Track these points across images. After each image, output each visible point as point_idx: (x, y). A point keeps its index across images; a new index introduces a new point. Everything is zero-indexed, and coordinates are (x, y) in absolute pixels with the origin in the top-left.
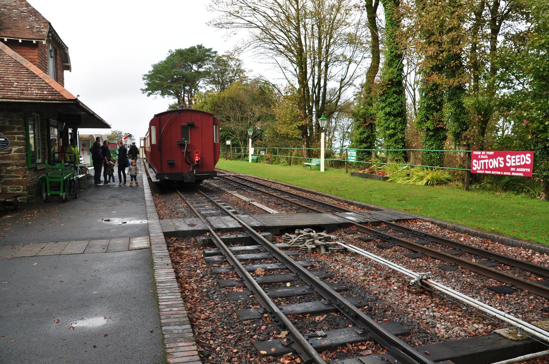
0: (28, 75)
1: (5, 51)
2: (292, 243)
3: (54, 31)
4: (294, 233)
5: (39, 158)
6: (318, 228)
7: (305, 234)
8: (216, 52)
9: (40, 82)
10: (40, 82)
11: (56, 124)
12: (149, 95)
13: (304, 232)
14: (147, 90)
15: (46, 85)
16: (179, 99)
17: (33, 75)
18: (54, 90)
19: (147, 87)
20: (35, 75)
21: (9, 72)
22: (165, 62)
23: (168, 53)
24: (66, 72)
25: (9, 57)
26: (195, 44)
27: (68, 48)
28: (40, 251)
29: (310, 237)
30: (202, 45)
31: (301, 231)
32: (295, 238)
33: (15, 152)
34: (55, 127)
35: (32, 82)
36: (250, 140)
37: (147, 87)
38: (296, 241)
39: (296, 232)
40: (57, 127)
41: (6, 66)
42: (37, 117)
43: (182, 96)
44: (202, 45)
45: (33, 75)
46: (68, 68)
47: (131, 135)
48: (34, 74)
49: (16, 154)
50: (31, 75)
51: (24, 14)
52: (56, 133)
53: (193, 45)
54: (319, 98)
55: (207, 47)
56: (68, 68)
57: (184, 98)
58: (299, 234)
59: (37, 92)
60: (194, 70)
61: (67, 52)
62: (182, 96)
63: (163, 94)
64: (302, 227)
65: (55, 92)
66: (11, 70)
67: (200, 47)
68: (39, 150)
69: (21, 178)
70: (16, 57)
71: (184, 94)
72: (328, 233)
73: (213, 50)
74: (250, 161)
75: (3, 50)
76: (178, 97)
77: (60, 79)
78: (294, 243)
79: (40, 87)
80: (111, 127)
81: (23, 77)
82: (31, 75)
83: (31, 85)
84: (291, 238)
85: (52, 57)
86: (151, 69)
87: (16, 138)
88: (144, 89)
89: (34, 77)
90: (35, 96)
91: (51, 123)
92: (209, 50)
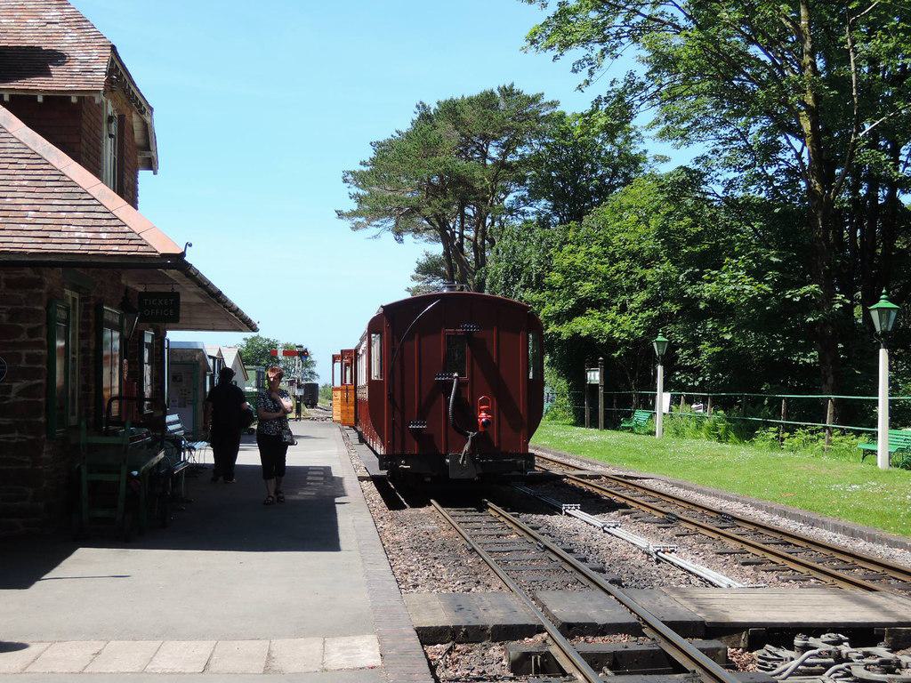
0: (63, 189)
1: (9, 130)
2: (785, 674)
3: (123, 66)
4: (791, 647)
5: (73, 414)
6: (862, 635)
7: (824, 648)
8: (554, 104)
9: (92, 208)
10: (92, 208)
11: (117, 320)
12: (356, 227)
13: (821, 643)
14: (354, 214)
15: (107, 216)
16: (447, 248)
17: (74, 190)
18: (126, 229)
19: (354, 206)
20: (80, 190)
21: (16, 183)
22: (408, 135)
23: (416, 110)
24: (144, 176)
25: (18, 145)
26: (493, 84)
27: (152, 109)
28: (92, 661)
29: (839, 658)
30: (512, 85)
31: (812, 641)
32: (792, 659)
33: (19, 394)
34: (113, 327)
35: (73, 208)
36: (660, 369)
37: (354, 206)
38: (796, 669)
39: (798, 641)
40: (119, 328)
41: (12, 166)
42: (74, 300)
43: (457, 235)
44: (512, 85)
45: (74, 190)
46: (151, 164)
47: (306, 351)
48: (78, 186)
49: (21, 399)
50: (70, 189)
51: (54, 26)
52: (117, 344)
53: (488, 88)
54: (874, 240)
55: (529, 91)
56: (151, 164)
57: (461, 245)
58: (805, 648)
59: (83, 235)
60: (492, 159)
61: (148, 120)
62: (457, 235)
63: (398, 233)
64: (815, 630)
65: (129, 236)
66: (22, 177)
67: (508, 92)
68: (73, 391)
69: (28, 467)
70: (35, 143)
71: (462, 228)
72: (894, 649)
73: (547, 99)
74: (882, 460)
75: (4, 126)
76: (447, 239)
77: (128, 191)
78: (791, 675)
79: (90, 222)
80: (258, 326)
81: (51, 196)
82: (70, 189)
83: (70, 215)
84: (781, 660)
85: (111, 136)
86: (369, 154)
87: (24, 358)
88: (346, 210)
89: (78, 196)
90: (78, 247)
91: (105, 317)
92: (534, 100)
